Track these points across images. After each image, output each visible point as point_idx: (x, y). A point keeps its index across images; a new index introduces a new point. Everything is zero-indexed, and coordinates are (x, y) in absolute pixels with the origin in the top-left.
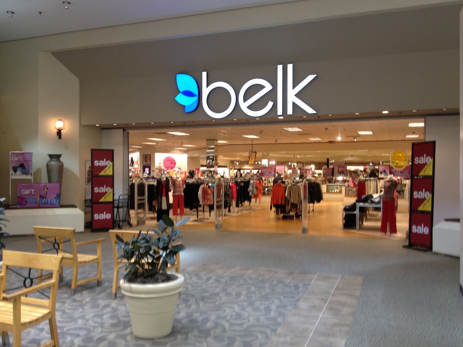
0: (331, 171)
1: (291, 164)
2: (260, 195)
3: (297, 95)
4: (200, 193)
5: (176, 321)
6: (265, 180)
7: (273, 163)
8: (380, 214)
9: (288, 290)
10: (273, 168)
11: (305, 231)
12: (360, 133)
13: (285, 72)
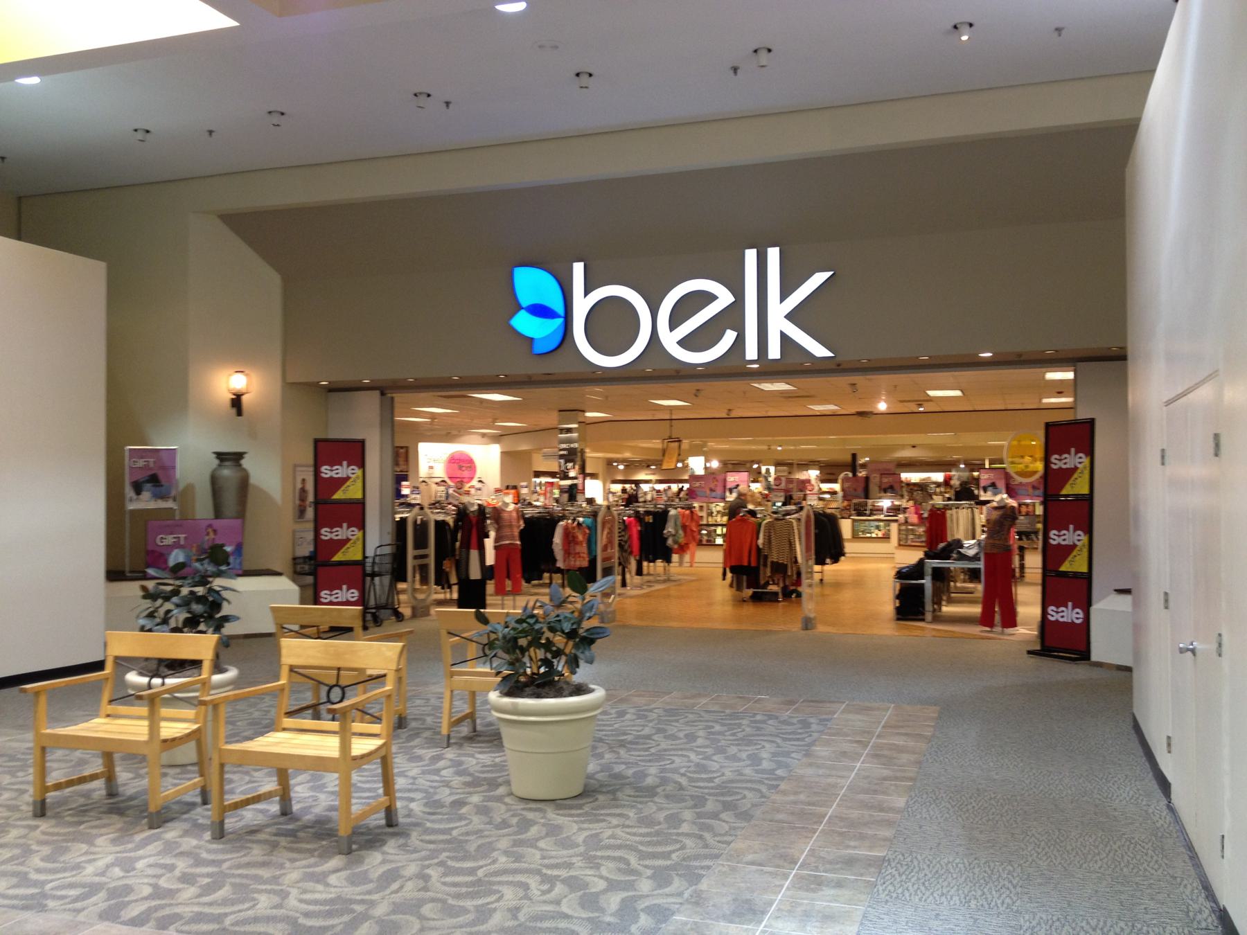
0: (862, 485)
1: (759, 468)
2: (692, 546)
3: (790, 317)
4: (558, 539)
5: (590, 777)
6: (701, 507)
7: (715, 464)
8: (980, 588)
9: (789, 728)
10: (720, 477)
11: (808, 624)
12: (932, 393)
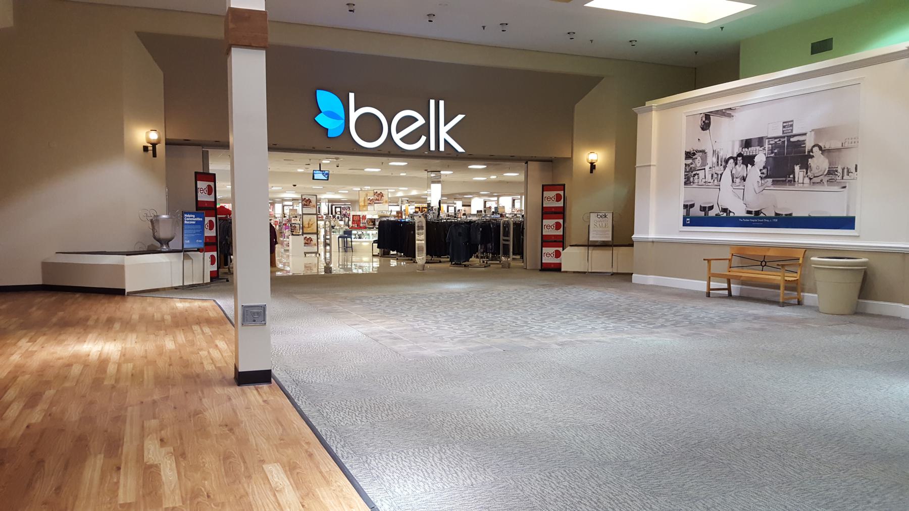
13: (437, 107)
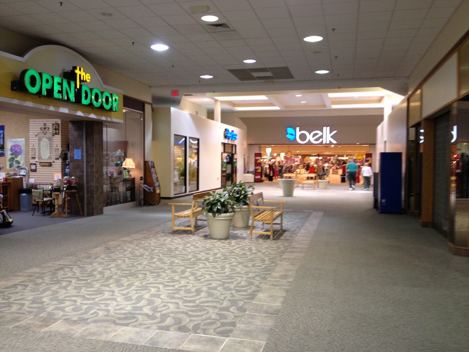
3: (332, 137)
13: (326, 130)
